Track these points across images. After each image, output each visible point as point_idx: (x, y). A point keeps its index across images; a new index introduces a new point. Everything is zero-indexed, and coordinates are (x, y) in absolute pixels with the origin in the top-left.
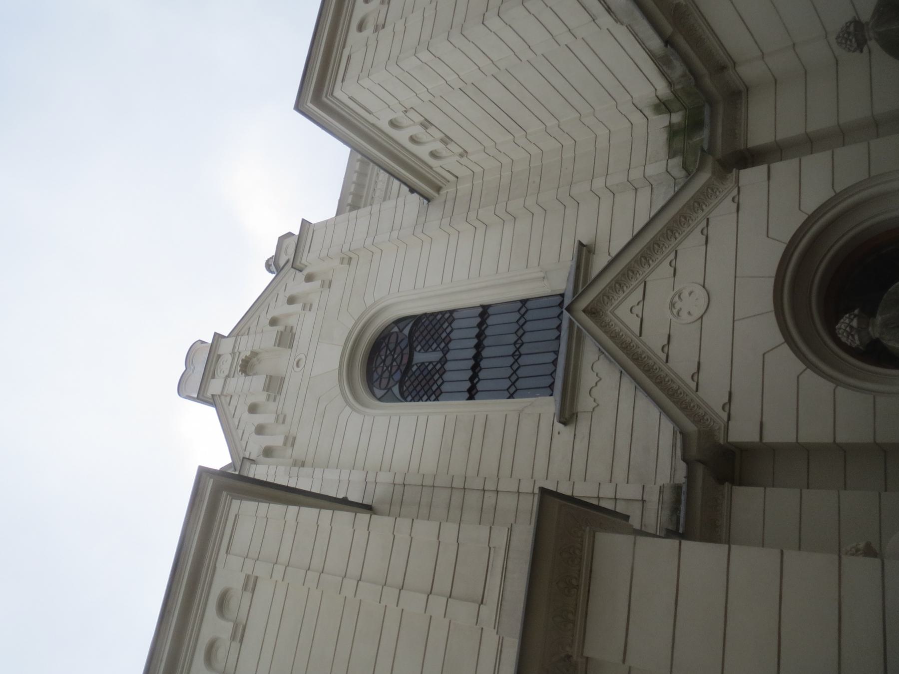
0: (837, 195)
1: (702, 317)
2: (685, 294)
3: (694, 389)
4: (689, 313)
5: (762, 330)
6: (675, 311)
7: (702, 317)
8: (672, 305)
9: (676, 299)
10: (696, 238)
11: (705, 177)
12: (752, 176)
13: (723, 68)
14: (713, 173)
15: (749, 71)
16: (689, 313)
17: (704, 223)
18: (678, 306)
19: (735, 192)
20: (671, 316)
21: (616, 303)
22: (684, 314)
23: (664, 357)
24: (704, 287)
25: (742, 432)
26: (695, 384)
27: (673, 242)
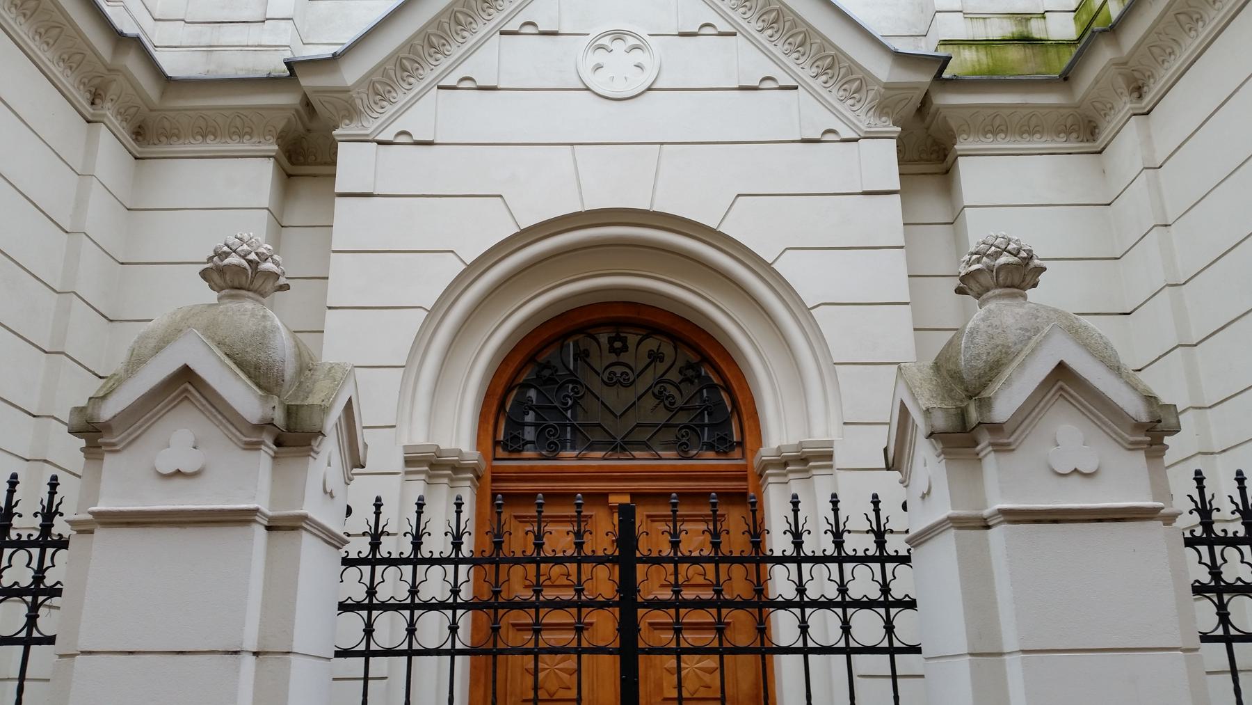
0: (768, 266)
1: (588, 89)
2: (637, 56)
3: (506, 28)
4: (599, 67)
5: (549, 190)
6: (606, 41)
7: (588, 89)
8: (618, 35)
9: (631, 41)
10: (754, 65)
11: (882, 70)
12: (881, 161)
13: (1138, 91)
14: (888, 87)
15: (1129, 144)
16: (599, 67)
17: (786, 80)
18: (619, 46)
19: (846, 133)
20: (594, 33)
21: (472, 40)
22: (600, 56)
23: (513, 25)
24: (649, 89)
25: (354, 166)
26: (454, 83)
27: (753, 27)
